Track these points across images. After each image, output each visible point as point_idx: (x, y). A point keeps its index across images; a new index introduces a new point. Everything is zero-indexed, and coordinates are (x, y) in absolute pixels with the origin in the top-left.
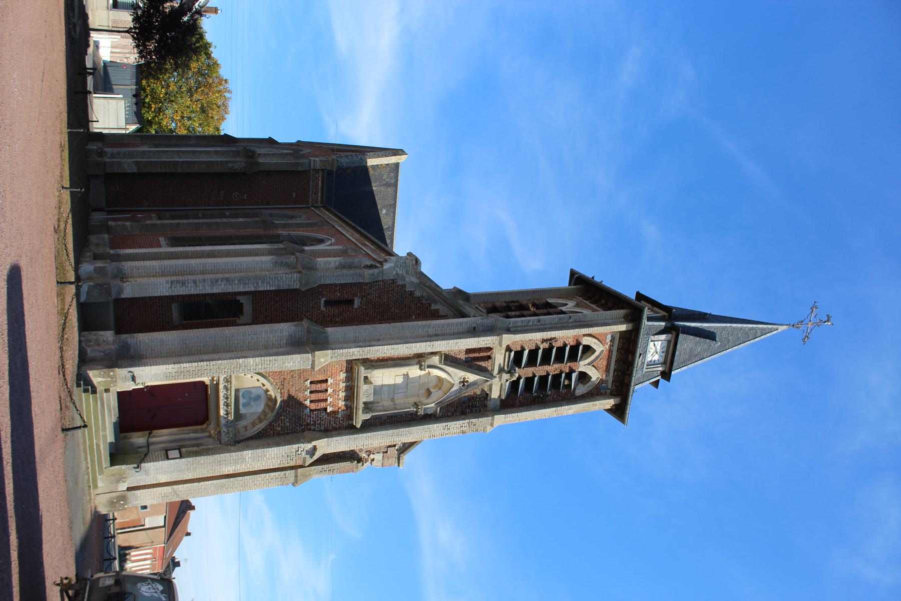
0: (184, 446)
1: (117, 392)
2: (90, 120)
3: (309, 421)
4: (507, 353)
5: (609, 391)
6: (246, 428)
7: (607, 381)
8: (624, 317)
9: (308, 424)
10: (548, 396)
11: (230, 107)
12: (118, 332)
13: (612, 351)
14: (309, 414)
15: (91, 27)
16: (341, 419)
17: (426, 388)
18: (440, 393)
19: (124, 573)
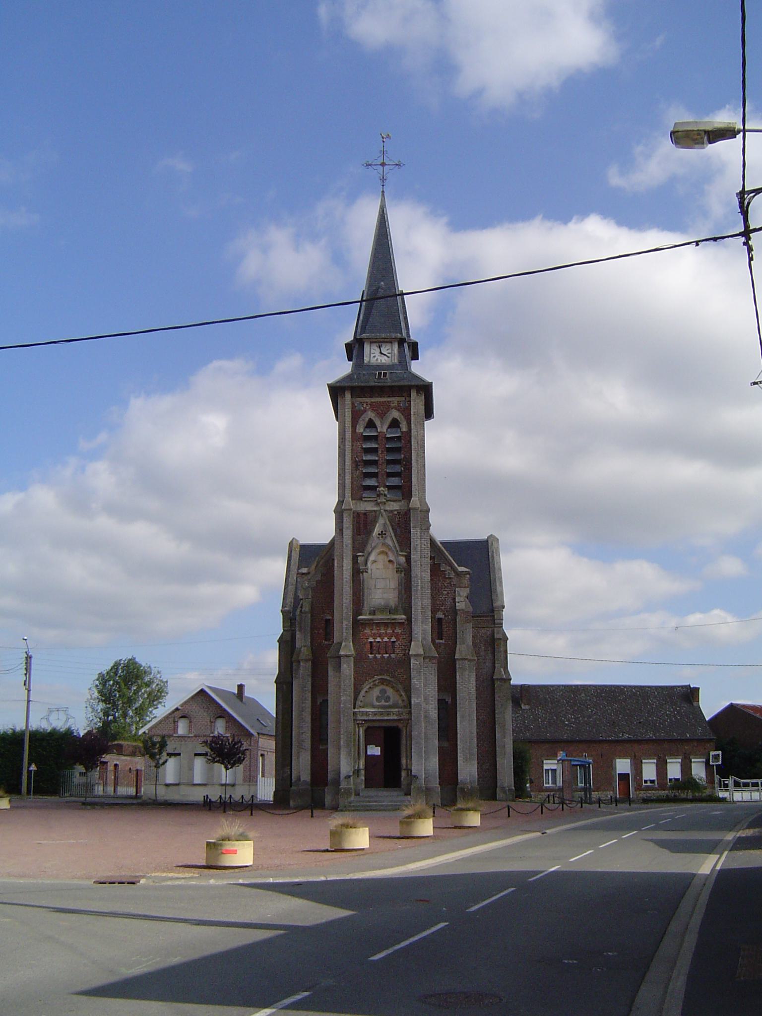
0: (131, 797)
1: (365, 787)
2: (314, 811)
3: (402, 654)
4: (363, 499)
5: (407, 398)
6: (403, 701)
7: (398, 402)
8: (342, 398)
9: (404, 655)
10: (405, 457)
11: (168, 746)
12: (327, 785)
13: (372, 402)
14: (395, 655)
15: (273, 738)
16: (402, 630)
17: (388, 563)
18: (390, 553)
19: (9, 798)
